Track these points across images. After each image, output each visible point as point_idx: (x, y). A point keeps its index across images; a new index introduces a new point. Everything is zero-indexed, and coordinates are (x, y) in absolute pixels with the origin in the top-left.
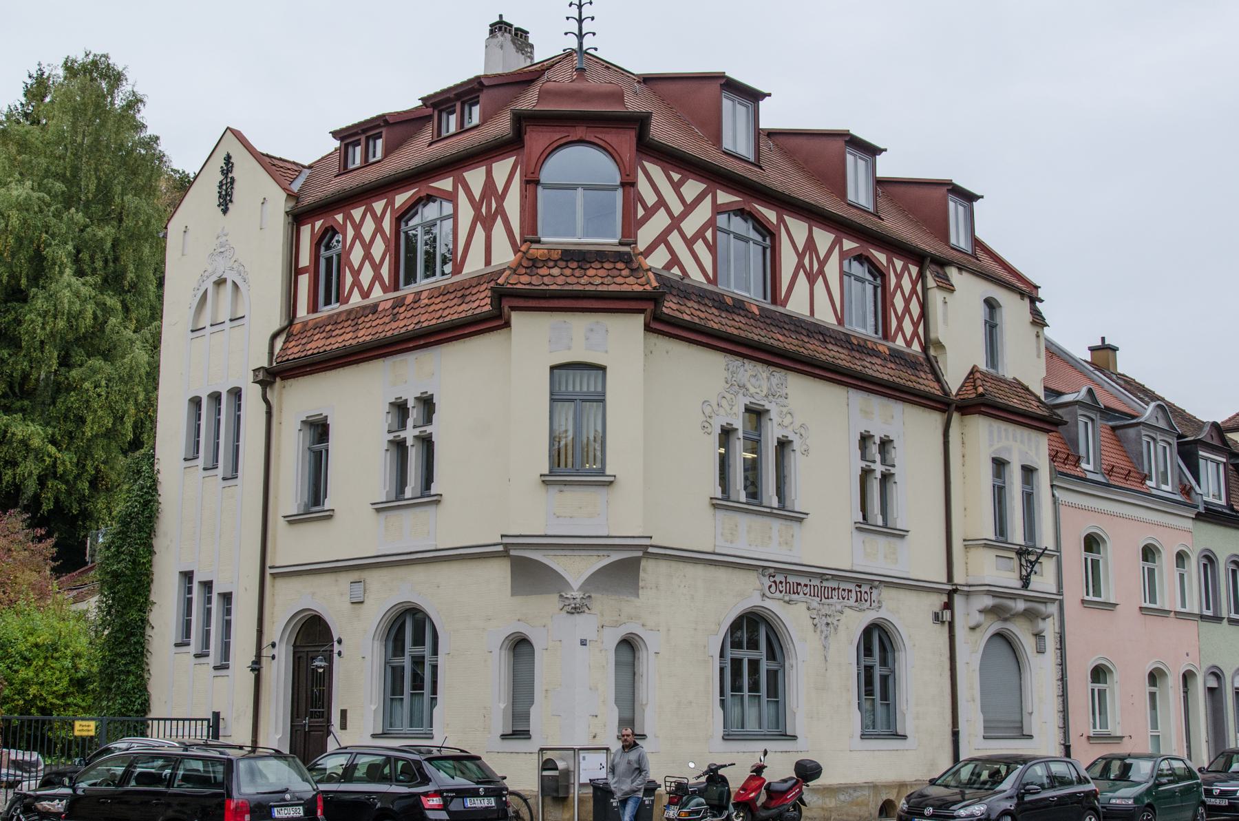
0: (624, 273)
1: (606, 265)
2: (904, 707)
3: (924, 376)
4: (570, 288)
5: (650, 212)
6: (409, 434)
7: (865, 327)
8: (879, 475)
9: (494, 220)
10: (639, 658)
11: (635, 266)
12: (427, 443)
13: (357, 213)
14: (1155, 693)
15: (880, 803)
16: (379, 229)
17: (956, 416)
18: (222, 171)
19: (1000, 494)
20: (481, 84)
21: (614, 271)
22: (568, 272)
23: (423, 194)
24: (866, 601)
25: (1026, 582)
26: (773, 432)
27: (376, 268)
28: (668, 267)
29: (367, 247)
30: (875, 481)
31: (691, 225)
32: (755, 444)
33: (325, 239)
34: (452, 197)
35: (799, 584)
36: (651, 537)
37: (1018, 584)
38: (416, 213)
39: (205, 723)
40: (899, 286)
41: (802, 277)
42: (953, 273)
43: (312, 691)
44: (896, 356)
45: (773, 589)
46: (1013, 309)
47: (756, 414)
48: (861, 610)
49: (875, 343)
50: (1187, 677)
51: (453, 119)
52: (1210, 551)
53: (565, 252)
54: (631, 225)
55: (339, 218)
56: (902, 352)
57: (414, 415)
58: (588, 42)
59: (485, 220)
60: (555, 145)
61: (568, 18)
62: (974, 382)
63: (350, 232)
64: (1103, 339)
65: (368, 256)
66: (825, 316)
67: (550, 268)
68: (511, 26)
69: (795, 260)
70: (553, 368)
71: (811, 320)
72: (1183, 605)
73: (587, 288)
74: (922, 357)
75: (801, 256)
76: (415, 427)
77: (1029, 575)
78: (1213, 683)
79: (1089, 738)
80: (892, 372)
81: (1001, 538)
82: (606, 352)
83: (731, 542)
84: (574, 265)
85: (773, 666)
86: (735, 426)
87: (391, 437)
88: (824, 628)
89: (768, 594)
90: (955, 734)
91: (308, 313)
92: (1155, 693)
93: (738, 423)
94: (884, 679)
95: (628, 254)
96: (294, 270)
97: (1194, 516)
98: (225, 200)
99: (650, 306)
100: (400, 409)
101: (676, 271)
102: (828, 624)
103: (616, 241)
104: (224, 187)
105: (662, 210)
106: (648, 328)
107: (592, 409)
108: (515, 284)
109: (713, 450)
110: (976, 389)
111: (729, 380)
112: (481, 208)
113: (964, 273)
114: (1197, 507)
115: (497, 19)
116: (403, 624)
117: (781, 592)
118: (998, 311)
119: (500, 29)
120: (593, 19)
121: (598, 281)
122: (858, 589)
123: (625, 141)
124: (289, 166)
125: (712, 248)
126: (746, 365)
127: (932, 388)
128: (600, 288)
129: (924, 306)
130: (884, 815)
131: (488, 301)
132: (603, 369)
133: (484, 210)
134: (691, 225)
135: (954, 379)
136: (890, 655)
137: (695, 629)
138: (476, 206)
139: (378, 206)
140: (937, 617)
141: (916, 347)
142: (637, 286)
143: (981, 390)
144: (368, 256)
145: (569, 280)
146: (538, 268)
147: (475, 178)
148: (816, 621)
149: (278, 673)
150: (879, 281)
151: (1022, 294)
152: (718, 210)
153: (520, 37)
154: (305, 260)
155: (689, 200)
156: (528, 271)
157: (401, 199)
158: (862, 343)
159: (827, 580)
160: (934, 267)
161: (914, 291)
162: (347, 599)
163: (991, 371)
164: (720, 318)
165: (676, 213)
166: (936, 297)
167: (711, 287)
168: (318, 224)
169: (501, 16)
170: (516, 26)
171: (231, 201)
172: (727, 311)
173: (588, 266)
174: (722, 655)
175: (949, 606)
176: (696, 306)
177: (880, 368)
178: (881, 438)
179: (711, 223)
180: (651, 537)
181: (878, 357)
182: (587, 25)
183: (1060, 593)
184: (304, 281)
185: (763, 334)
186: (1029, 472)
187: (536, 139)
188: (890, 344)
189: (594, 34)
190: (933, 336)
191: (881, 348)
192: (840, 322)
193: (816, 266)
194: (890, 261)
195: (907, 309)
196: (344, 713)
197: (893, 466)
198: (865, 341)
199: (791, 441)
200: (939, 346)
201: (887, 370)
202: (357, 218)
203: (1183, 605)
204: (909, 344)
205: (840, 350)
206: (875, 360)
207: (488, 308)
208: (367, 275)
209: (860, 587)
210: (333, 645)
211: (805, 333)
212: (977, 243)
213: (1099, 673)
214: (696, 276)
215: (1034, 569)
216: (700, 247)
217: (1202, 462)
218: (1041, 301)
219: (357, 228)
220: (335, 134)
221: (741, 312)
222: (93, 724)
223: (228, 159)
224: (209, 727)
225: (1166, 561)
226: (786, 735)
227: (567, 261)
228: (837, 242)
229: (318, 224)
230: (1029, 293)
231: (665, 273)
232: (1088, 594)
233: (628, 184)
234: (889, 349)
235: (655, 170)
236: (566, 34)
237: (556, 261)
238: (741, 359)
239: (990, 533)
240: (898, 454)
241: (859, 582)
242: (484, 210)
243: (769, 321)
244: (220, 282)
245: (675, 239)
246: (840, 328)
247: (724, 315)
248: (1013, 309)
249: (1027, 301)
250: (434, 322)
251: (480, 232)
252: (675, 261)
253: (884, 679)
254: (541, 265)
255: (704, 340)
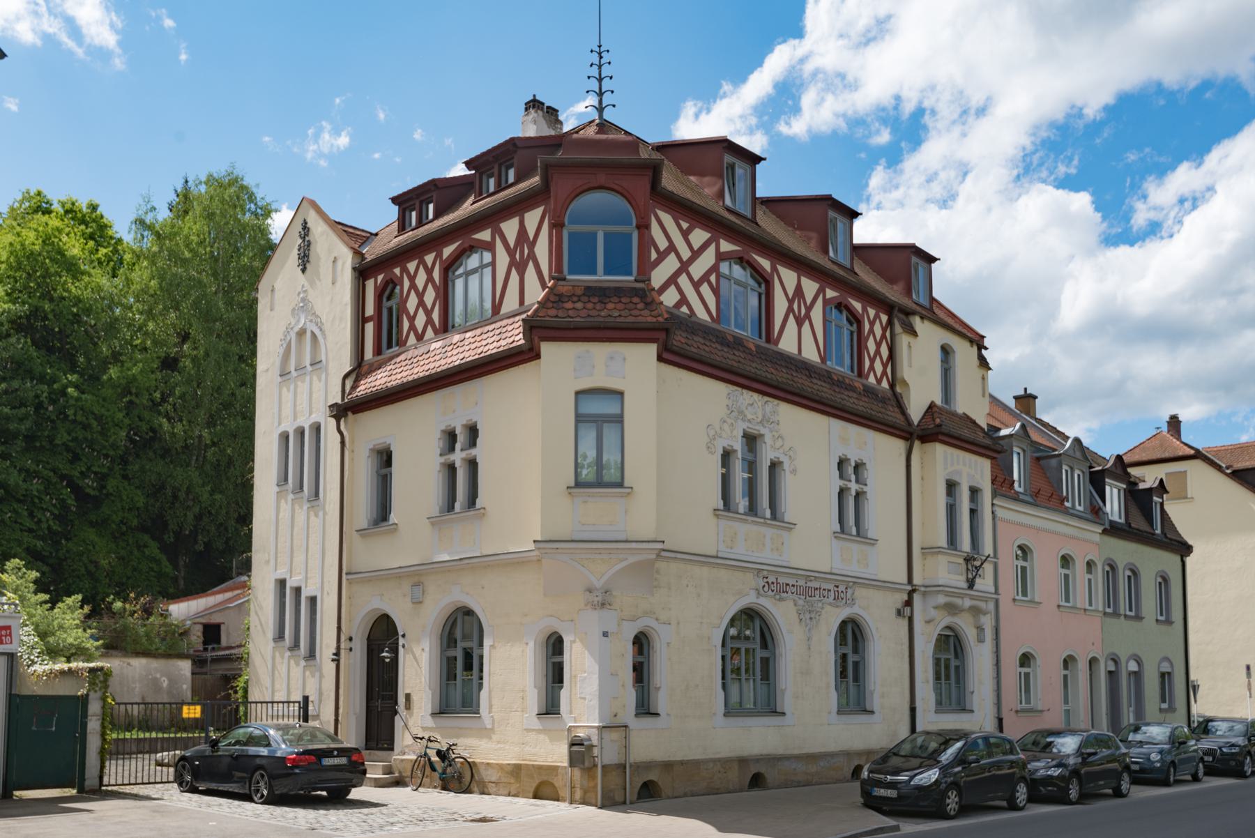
0: (639, 306)
1: (624, 300)
2: (872, 688)
3: (891, 409)
4: (592, 319)
5: (662, 256)
6: (458, 457)
7: (841, 364)
8: (854, 493)
9: (526, 265)
10: (653, 648)
11: (649, 300)
12: (473, 464)
13: (412, 266)
14: (1029, 673)
15: (852, 768)
16: (430, 279)
17: (917, 443)
18: (300, 236)
19: (951, 510)
20: (515, 145)
21: (631, 304)
22: (590, 306)
23: (466, 245)
24: (842, 599)
25: (971, 583)
26: (767, 454)
27: (428, 313)
28: (678, 305)
29: (420, 296)
30: (850, 497)
31: (698, 269)
32: (751, 466)
33: (387, 291)
34: (490, 247)
35: (787, 585)
36: (663, 542)
37: (965, 585)
38: (461, 265)
39: (297, 705)
40: (872, 331)
41: (792, 321)
42: (917, 322)
43: (383, 677)
44: (869, 392)
45: (766, 589)
46: (964, 353)
47: (751, 440)
48: (837, 606)
49: (852, 380)
50: (1093, 662)
51: (492, 181)
52: (1113, 561)
53: (588, 288)
54: (646, 268)
55: (397, 271)
56: (873, 388)
57: (461, 439)
58: (609, 115)
59: (519, 266)
60: (578, 191)
61: (589, 77)
62: (932, 415)
63: (406, 283)
64: (1026, 389)
65: (421, 303)
66: (811, 354)
67: (574, 302)
68: (543, 104)
69: (786, 304)
70: (577, 393)
71: (799, 357)
72: (1090, 604)
73: (607, 320)
74: (889, 394)
75: (791, 302)
76: (462, 450)
77: (974, 578)
78: (1112, 668)
79: (1017, 712)
80: (867, 405)
81: (952, 547)
82: (624, 378)
83: (731, 548)
84: (596, 300)
85: (765, 654)
86: (735, 448)
87: (442, 460)
88: (808, 621)
89: (762, 592)
90: (913, 710)
91: (374, 355)
92: (1029, 673)
93: (738, 445)
94: (856, 664)
95: (643, 290)
96: (360, 320)
97: (1100, 531)
98: (304, 260)
99: (662, 336)
100: (451, 436)
101: (684, 309)
102: (811, 618)
103: (632, 278)
104: (302, 250)
105: (673, 255)
106: (660, 358)
107: (610, 433)
108: (544, 317)
109: (716, 471)
110: (934, 421)
111: (730, 406)
112: (515, 254)
113: (925, 322)
114: (1103, 525)
115: (532, 98)
116: (455, 620)
117: (773, 591)
118: (951, 355)
119: (534, 107)
120: (608, 51)
121: (616, 314)
122: (836, 589)
123: (641, 186)
124: (359, 233)
125: (716, 291)
126: (742, 394)
127: (899, 419)
128: (618, 320)
129: (891, 350)
130: (855, 777)
131: (521, 336)
132: (621, 394)
133: (517, 256)
134: (698, 269)
135: (916, 412)
136: (860, 644)
137: (701, 623)
138: (511, 253)
139: (429, 259)
140: (899, 613)
141: (885, 384)
142: (651, 318)
143: (938, 421)
144: (421, 303)
145: (591, 313)
146: (563, 302)
147: (510, 228)
148: (802, 616)
149: (356, 662)
150: (854, 328)
151: (971, 341)
152: (721, 257)
153: (552, 114)
154: (370, 310)
155: (696, 247)
156: (555, 305)
157: (448, 251)
158: (841, 379)
159: (811, 581)
160: (902, 316)
161: (883, 336)
162: (408, 599)
163: (945, 406)
164: (723, 353)
165: (685, 258)
166: (904, 340)
167: (715, 326)
168: (380, 278)
169: (534, 96)
170: (547, 104)
171: (308, 261)
172: (728, 346)
173: (608, 300)
174: (723, 645)
175: (909, 603)
176: (702, 340)
177: (856, 401)
178: (856, 461)
179: (714, 269)
180: (663, 542)
181: (855, 392)
182: (606, 84)
183: (996, 592)
184: (370, 328)
185: (759, 367)
186: (974, 492)
187: (561, 186)
188: (864, 381)
189: (614, 106)
190: (899, 375)
191: (856, 384)
192: (823, 360)
193: (803, 311)
194: (864, 309)
195: (878, 352)
196: (408, 697)
197: (866, 485)
198: (843, 377)
199: (782, 462)
200: (905, 383)
201: (861, 403)
202: (412, 270)
203: (1090, 604)
204: (879, 381)
205: (823, 384)
206: (851, 394)
207: (522, 342)
208: (420, 320)
209: (837, 587)
210: (398, 639)
211: (793, 368)
212: (933, 300)
213: (1026, 659)
214: (702, 314)
215: (979, 573)
216: (705, 289)
217: (1108, 489)
218: (986, 348)
219: (412, 279)
220: (395, 200)
221: (741, 349)
222: (198, 708)
223: (305, 227)
224: (300, 708)
225: (1080, 566)
226: (776, 712)
227: (589, 296)
228: (821, 291)
229: (380, 278)
230: (978, 342)
231: (675, 311)
232: (1018, 595)
233: (644, 227)
234: (863, 385)
235: (666, 218)
236: (588, 92)
237: (579, 296)
238: (740, 389)
239: (943, 541)
240: (870, 474)
241: (837, 583)
242: (517, 256)
243: (763, 357)
244: (301, 333)
245: (683, 280)
246: (823, 366)
247: (725, 350)
248: (964, 353)
249: (975, 348)
250: (477, 357)
251: (514, 276)
252: (683, 300)
253: (856, 664)
254: (566, 299)
255: (709, 370)
